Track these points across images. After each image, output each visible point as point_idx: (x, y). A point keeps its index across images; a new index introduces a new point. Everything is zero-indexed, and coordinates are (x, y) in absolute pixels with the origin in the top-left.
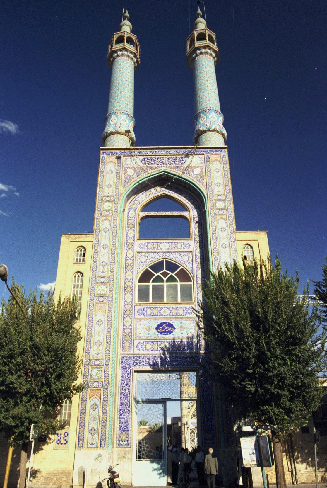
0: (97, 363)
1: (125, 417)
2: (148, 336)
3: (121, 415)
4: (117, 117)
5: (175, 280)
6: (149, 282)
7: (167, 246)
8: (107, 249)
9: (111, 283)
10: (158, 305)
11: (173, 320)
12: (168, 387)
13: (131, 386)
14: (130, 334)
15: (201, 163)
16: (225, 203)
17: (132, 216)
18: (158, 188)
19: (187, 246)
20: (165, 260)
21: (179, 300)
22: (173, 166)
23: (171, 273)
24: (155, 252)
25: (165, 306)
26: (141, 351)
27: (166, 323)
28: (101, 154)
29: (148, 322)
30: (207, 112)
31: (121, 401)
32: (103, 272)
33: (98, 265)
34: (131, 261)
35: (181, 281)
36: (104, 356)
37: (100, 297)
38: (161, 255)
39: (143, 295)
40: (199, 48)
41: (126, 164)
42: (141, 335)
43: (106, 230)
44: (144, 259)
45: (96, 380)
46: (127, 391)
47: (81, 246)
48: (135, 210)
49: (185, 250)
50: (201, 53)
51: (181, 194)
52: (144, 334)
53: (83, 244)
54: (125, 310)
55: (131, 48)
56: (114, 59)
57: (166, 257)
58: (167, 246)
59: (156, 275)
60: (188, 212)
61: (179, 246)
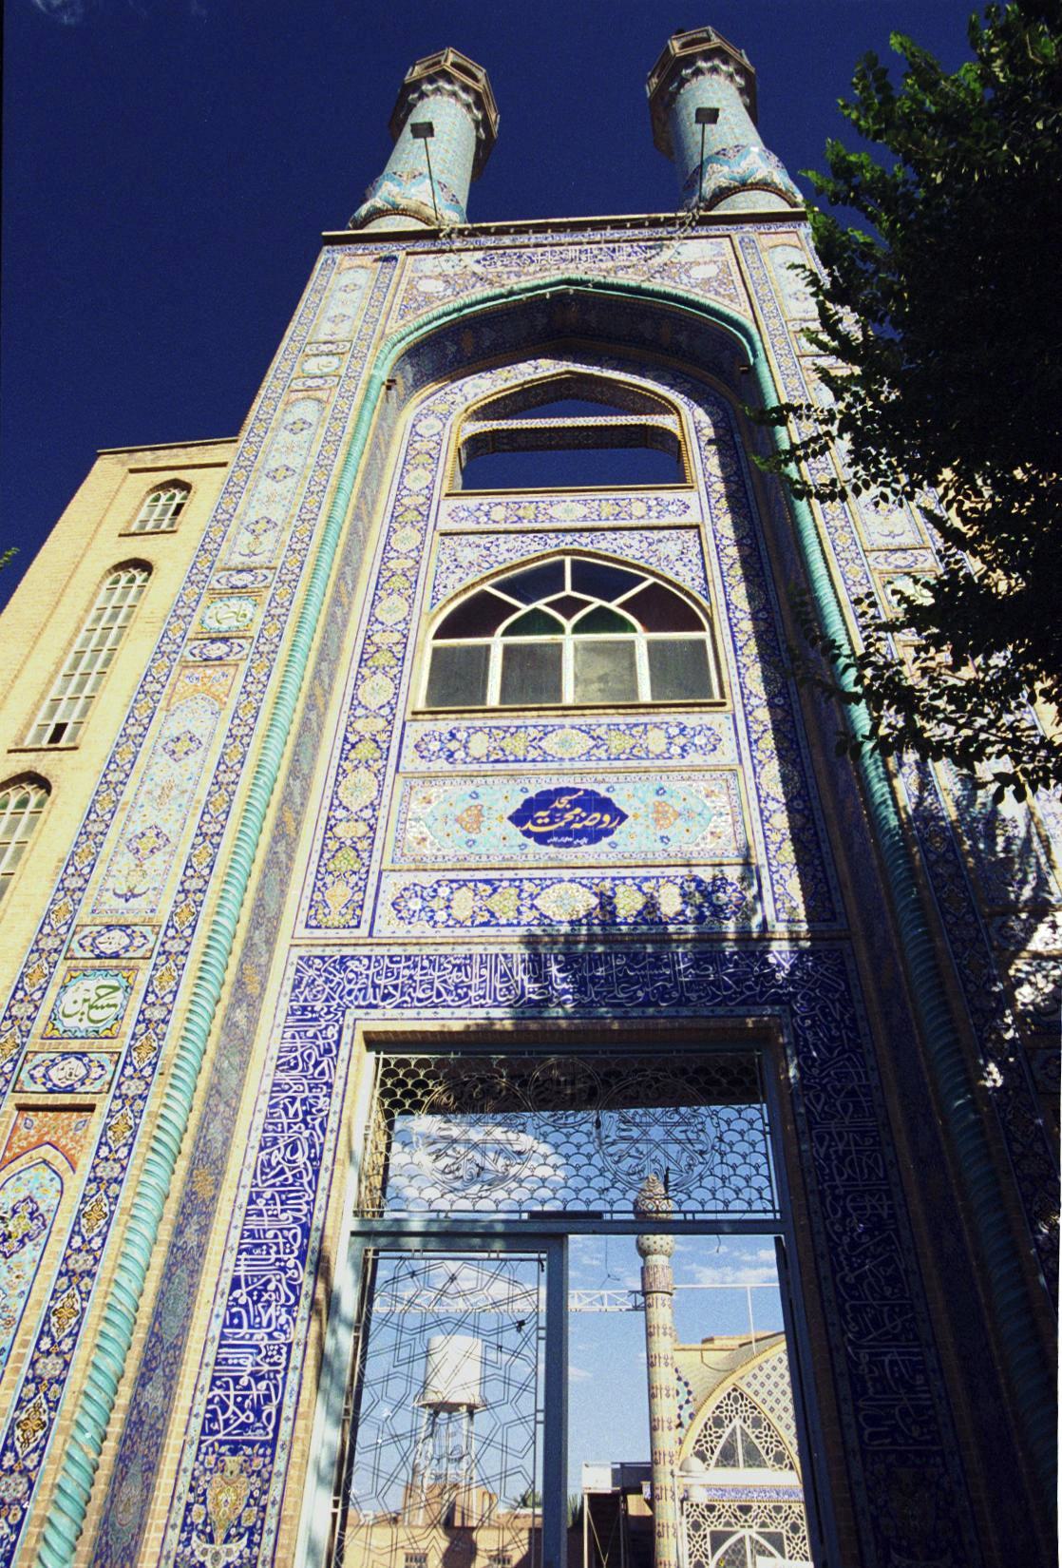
0: (115, 941)
1: (260, 1335)
2: (465, 851)
3: (233, 1321)
5: (623, 626)
6: (489, 631)
7: (581, 510)
9: (283, 590)
10: (530, 718)
11: (612, 778)
13: (332, 1123)
14: (363, 845)
18: (548, 362)
19: (700, 740)
20: (568, 560)
21: (645, 695)
23: (597, 602)
25: (567, 721)
26: (421, 928)
27: (576, 791)
29: (470, 788)
31: (254, 1223)
35: (650, 627)
36: (165, 908)
37: (213, 641)
39: (455, 684)
42: (427, 850)
45: (75, 1045)
46: (301, 1158)
49: (663, 522)
51: (643, 376)
52: (448, 845)
54: (353, 739)
58: (581, 510)
59: (525, 609)
60: (675, 417)
61: (639, 509)
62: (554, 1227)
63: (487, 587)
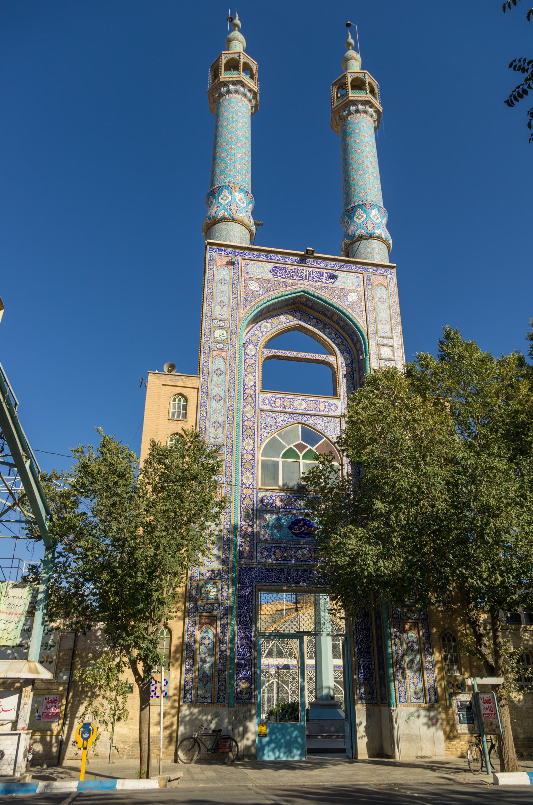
4: (231, 194)
8: (221, 402)
12: (306, 615)
15: (358, 286)
16: (393, 351)
17: (251, 354)
22: (318, 285)
23: (310, 447)
24: (286, 413)
28: (208, 250)
30: (368, 206)
32: (216, 438)
33: (208, 425)
34: (252, 424)
38: (296, 418)
40: (354, 103)
41: (247, 273)
43: (219, 372)
44: (270, 421)
46: (248, 619)
47: (180, 394)
48: (256, 345)
50: (357, 111)
53: (184, 391)
54: (244, 496)
55: (252, 84)
56: (221, 96)
57: (303, 421)
58: (304, 405)
62: (301, 634)
63: (275, 435)
